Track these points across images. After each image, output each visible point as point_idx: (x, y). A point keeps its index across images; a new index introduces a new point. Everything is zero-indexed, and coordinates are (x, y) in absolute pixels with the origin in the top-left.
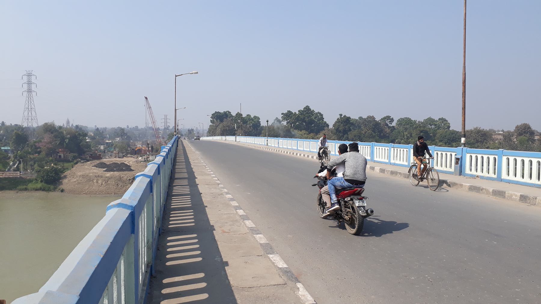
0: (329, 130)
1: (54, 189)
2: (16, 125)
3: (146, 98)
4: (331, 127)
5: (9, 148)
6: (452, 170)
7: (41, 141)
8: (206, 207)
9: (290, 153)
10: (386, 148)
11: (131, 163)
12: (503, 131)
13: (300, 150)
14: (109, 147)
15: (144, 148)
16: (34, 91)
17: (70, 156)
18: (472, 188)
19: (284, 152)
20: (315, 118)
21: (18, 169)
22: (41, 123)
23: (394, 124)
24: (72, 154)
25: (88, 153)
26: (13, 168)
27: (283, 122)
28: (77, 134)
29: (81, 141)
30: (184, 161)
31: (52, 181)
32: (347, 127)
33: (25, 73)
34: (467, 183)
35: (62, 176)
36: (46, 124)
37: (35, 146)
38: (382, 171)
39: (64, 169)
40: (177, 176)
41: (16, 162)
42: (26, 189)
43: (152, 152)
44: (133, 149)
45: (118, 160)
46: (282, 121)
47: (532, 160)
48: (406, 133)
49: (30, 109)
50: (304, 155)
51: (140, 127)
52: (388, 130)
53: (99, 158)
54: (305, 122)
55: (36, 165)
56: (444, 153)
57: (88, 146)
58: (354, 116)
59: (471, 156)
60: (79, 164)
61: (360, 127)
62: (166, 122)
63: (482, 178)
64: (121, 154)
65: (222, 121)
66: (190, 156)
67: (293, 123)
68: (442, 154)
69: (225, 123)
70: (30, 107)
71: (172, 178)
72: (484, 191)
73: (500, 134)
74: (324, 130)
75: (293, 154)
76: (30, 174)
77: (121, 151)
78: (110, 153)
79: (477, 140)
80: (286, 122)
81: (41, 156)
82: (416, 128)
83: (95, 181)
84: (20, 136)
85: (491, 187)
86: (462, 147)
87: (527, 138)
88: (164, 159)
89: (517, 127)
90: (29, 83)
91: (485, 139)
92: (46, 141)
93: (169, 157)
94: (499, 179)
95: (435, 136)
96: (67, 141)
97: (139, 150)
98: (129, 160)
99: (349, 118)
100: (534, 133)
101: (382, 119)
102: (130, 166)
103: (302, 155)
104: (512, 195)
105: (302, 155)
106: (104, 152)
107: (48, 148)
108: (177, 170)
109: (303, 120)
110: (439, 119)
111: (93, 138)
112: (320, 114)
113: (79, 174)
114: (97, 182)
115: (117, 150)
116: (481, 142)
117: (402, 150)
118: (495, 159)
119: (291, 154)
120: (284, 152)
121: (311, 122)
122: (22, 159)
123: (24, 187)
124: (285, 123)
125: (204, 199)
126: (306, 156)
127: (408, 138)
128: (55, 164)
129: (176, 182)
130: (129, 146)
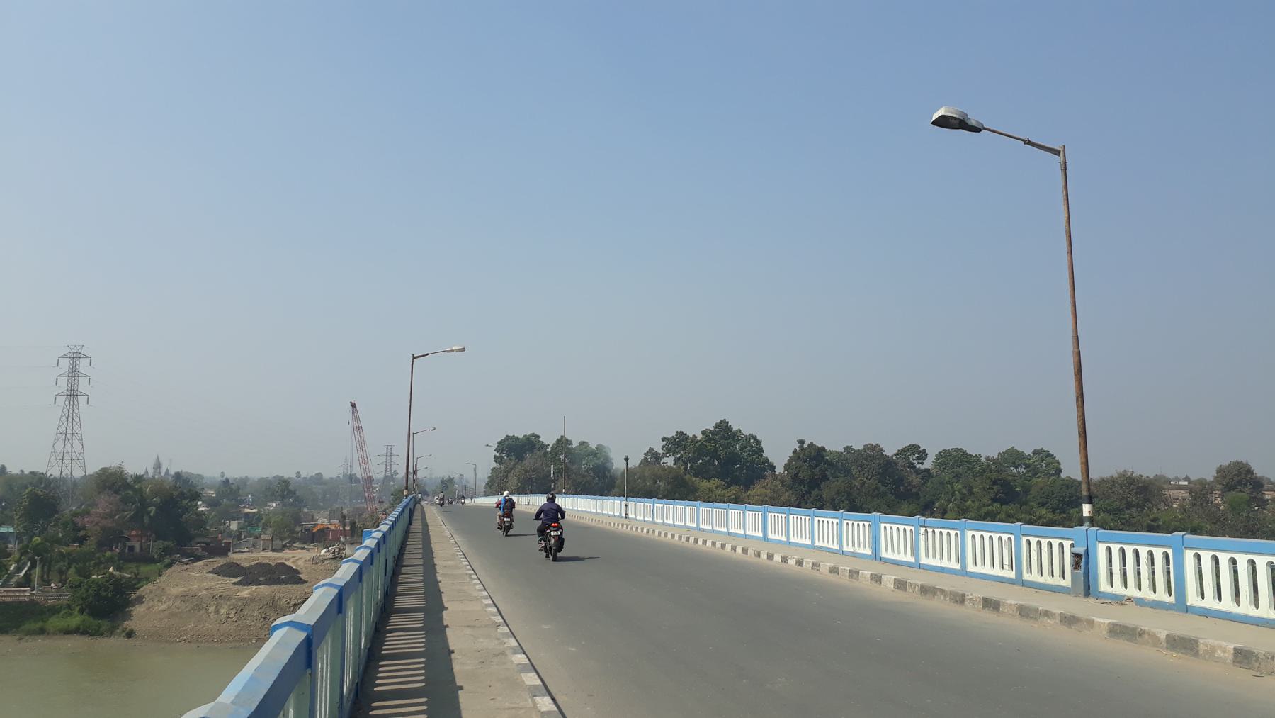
0: (775, 477)
1: (111, 632)
2: (33, 473)
3: (354, 405)
4: (780, 469)
5: (11, 530)
6: (1067, 582)
7: (88, 513)
8: (461, 688)
9: (680, 538)
10: (908, 528)
11: (301, 563)
12: (1187, 479)
13: (704, 530)
14: (250, 523)
15: (335, 525)
16: (83, 394)
17: (156, 547)
18: (1117, 631)
19: (666, 535)
20: (742, 449)
21: (27, 581)
22: (93, 468)
23: (928, 464)
24: (161, 543)
25: (199, 540)
26: (15, 579)
27: (664, 460)
28: (175, 493)
29: (186, 510)
30: (421, 562)
31: (107, 609)
32: (817, 470)
33: (66, 351)
34: (1104, 618)
35: (134, 596)
36: (104, 470)
37: (74, 523)
38: (901, 585)
39: (140, 580)
40: (399, 603)
41: (25, 564)
42: (42, 631)
43: (352, 535)
44: (307, 530)
45: (270, 557)
46: (664, 456)
47: (1255, 560)
48: (958, 486)
49: (69, 432)
50: (714, 544)
51: (326, 476)
52: (915, 479)
53: (224, 551)
54: (718, 459)
55: (72, 570)
56: (1044, 542)
57: (201, 521)
58: (834, 443)
59: (1109, 550)
60: (176, 567)
61: (848, 471)
62: (388, 464)
63: (1141, 602)
64: (278, 543)
65: (520, 458)
66: (437, 548)
67: (689, 460)
68: (1039, 543)
69: (529, 460)
70: (69, 431)
71: (386, 610)
72: (1146, 636)
73: (1180, 488)
74: (764, 477)
75: (688, 539)
76: (55, 594)
77: (278, 535)
78: (251, 540)
79: (1128, 503)
80: (672, 458)
81: (85, 548)
82: (982, 473)
83: (211, 609)
84: (39, 501)
85: (1162, 626)
86: (1084, 528)
87: (1246, 497)
88: (360, 569)
89: (1220, 470)
90: (74, 375)
91: (1148, 500)
92: (100, 511)
93: (380, 560)
94: (1181, 606)
95: (1026, 491)
96: (153, 510)
97: (322, 531)
98: (297, 557)
99: (823, 449)
100: (1262, 486)
101: (899, 453)
102: (297, 572)
103: (709, 543)
104: (1213, 650)
105: (709, 543)
106: (239, 537)
107: (103, 529)
108: (401, 588)
109: (714, 455)
110: (1035, 452)
111: (212, 503)
112: (755, 439)
113: (175, 591)
114: (217, 612)
115: (270, 530)
116: (1138, 506)
117: (945, 532)
118: (1167, 556)
119: (684, 539)
120: (666, 535)
121: (733, 459)
122: (40, 555)
123: (40, 624)
124: (669, 461)
125: (457, 668)
126: (718, 545)
127: (963, 499)
128: (119, 569)
129: (396, 621)
130: (298, 521)
